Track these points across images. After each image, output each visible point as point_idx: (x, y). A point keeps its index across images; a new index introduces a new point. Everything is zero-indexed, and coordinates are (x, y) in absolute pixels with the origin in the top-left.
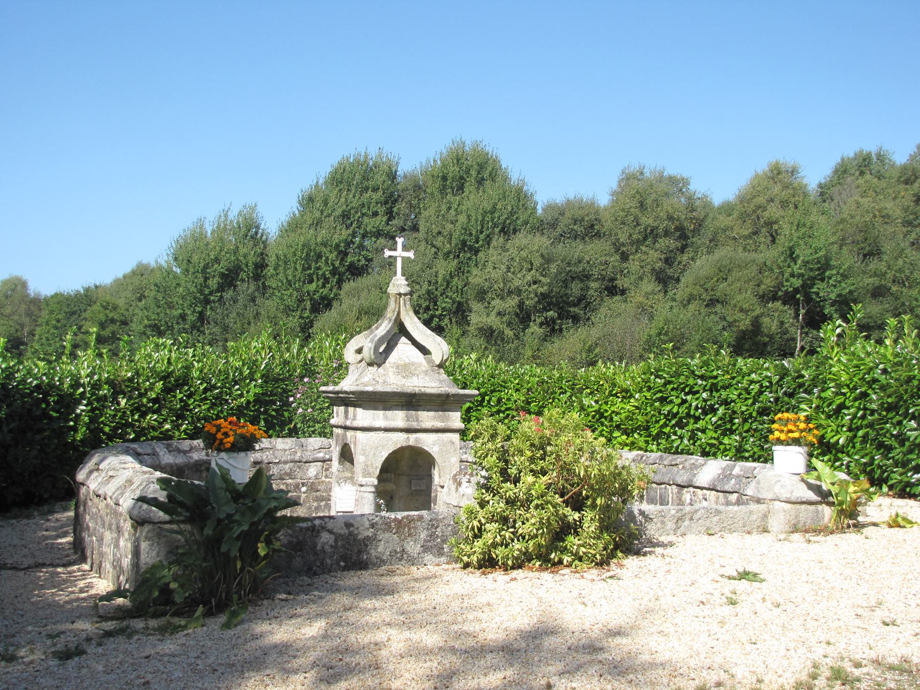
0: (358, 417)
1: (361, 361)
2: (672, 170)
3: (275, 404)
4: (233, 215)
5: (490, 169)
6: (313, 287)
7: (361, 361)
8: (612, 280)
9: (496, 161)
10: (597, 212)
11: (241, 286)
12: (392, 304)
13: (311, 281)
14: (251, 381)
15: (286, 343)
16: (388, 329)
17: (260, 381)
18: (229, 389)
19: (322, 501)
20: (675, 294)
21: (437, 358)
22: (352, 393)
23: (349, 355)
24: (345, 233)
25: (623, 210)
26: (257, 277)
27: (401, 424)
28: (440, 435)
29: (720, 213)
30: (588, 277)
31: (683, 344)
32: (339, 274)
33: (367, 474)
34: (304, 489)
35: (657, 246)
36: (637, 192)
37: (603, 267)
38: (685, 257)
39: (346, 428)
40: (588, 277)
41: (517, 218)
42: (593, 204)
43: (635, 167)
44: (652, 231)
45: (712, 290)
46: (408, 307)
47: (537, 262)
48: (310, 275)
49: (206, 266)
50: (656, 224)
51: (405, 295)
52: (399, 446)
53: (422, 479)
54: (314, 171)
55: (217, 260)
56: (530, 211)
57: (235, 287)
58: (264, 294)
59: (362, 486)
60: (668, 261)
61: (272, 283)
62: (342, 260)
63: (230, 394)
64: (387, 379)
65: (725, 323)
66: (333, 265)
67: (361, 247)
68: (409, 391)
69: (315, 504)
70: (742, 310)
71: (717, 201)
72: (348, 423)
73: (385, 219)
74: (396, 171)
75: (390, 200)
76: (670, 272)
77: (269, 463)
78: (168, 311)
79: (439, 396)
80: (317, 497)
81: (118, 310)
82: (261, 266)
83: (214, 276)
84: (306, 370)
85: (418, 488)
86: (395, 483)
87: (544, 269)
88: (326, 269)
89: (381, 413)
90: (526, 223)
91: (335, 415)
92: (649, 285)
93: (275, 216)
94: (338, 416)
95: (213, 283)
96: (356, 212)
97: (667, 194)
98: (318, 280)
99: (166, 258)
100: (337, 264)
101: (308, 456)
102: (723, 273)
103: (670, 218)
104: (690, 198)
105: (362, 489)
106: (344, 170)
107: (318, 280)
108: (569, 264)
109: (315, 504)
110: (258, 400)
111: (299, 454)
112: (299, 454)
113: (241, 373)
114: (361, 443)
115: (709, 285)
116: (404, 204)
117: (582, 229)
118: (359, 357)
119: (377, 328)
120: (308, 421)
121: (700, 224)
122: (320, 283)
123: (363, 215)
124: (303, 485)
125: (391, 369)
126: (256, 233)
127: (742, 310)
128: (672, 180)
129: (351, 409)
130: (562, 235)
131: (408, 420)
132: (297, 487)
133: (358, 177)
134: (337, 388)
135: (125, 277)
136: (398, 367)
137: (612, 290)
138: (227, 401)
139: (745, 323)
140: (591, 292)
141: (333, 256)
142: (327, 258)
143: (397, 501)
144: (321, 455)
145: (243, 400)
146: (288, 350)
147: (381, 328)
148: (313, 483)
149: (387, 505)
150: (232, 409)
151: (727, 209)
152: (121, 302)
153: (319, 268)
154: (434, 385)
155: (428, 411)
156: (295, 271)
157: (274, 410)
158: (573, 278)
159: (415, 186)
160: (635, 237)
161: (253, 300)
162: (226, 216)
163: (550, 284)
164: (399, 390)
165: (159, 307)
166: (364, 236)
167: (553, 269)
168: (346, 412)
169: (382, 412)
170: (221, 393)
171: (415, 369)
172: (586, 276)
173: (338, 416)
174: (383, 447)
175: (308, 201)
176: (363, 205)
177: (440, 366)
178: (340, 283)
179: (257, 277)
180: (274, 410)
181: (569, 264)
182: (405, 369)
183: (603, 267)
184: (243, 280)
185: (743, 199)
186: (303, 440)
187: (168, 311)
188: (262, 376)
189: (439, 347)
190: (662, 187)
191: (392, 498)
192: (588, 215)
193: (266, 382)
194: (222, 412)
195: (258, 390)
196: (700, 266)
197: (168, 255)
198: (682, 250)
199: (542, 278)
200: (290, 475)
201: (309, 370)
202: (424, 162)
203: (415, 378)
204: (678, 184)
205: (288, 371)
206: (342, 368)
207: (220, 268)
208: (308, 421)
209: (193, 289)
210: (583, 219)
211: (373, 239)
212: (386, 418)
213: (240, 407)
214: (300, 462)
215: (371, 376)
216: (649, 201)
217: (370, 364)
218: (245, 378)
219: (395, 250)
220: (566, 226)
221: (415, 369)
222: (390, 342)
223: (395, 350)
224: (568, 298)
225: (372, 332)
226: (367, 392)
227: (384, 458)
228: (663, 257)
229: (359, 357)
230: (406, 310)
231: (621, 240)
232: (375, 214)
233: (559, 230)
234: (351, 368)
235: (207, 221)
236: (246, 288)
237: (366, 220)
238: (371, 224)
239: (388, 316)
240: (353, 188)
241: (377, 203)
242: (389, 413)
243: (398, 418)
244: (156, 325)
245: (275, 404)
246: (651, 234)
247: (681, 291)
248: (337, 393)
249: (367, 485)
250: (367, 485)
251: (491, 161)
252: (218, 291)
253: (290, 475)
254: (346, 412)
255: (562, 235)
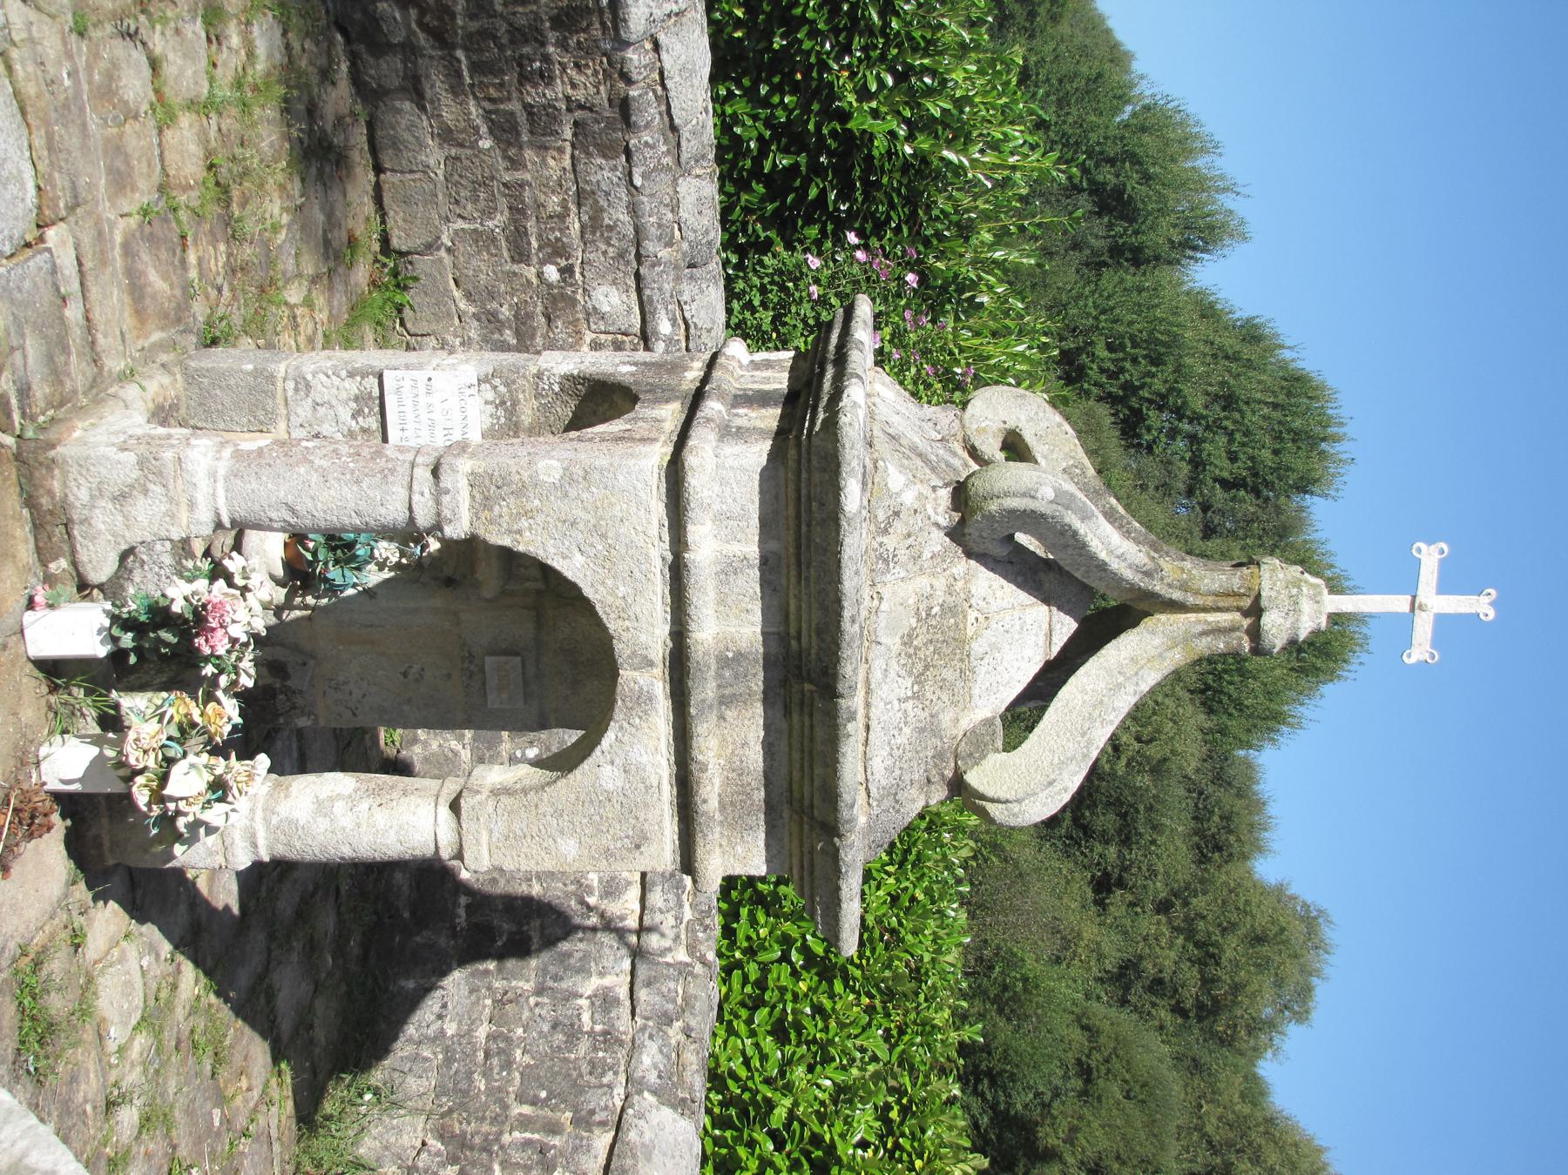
0: (731, 449)
1: (973, 452)
2: (1322, 992)
3: (841, 197)
4: (1227, 201)
5: (1319, 663)
6: (1102, 352)
7: (973, 452)
8: (1121, 884)
9: (1332, 675)
10: (1245, 857)
11: (1099, 226)
12: (1214, 578)
13: (1110, 348)
14: (907, 122)
15: (1022, 229)
16: (1114, 565)
17: (908, 150)
18: (883, 58)
19: (518, 334)
20: (1099, 998)
21: (992, 775)
22: (832, 423)
23: (997, 409)
24: (1197, 403)
25: (1247, 902)
26: (1116, 251)
27: (706, 633)
28: (668, 793)
29: (1245, 1077)
30: (1126, 842)
31: (1009, 1020)
32: (1125, 396)
33: (487, 490)
34: (552, 273)
35: (1185, 965)
36: (1283, 930)
37: (1144, 868)
38: (1164, 1015)
39: (697, 398)
40: (1126, 842)
41: (1230, 715)
42: (1260, 850)
43: (1328, 933)
44: (1212, 956)
45: (1109, 1071)
46: (1204, 646)
47: (1154, 751)
48: (1122, 347)
49: (1135, 160)
50: (1224, 962)
51: (1255, 633)
52: (612, 626)
53: (527, 696)
54: (1306, 346)
55: (1147, 178)
56: (1244, 738)
57: (1099, 215)
58: (1087, 265)
59: (435, 473)
60: (1157, 985)
61: (1109, 279)
62: (1150, 401)
63: (868, 61)
64: (898, 568)
65: (1047, 1098)
66: (1142, 387)
67: (1173, 433)
68: (847, 669)
69: (505, 312)
70: (1074, 1130)
71: (1266, 1068)
72: (713, 407)
73: (1225, 475)
74: (1312, 493)
75: (1254, 483)
76: (1138, 988)
77: (628, 153)
78: (1053, 98)
79: (830, 794)
80: (530, 316)
81: (1049, 24)
82: (1138, 258)
83: (1117, 176)
84: (944, 289)
85: (492, 682)
86: (504, 593)
87: (1140, 764)
88: (1132, 374)
89: (750, 548)
90: (1223, 731)
91: (762, 356)
92: (1114, 952)
93: (1223, 278)
94: (755, 366)
95: (1106, 175)
96: (1235, 422)
97: (1279, 984)
98: (1113, 361)
99: (1147, 93)
100: (1145, 393)
101: (661, 284)
102: (1141, 1092)
103: (1236, 988)
104: (1271, 1025)
105: (422, 474)
106: (1310, 398)
107: (1113, 361)
108: (1150, 809)
109: (505, 312)
110: (854, 144)
111: (664, 253)
112: (664, 253)
113: (929, 92)
114: (630, 461)
115: (1116, 1065)
116: (1252, 509)
117: (1214, 830)
118: (991, 447)
119: (1110, 515)
120: (783, 288)
121: (1226, 1042)
122: (1108, 365)
123: (1231, 435)
124: (567, 271)
125: (940, 583)
126: (1195, 248)
127: (1074, 1130)
128: (1305, 992)
129: (770, 417)
130: (1201, 793)
131: (724, 662)
132: (557, 251)
133: (1297, 423)
134: (861, 358)
135: (1108, 31)
136: (949, 610)
137: (1103, 886)
138: (847, 49)
139: (1049, 1137)
140: (1099, 848)
141: (1158, 385)
142: (1153, 376)
143: (438, 602)
144: (665, 327)
145: (851, 98)
146: (1002, 237)
147: (1115, 537)
148: (574, 302)
149: (419, 565)
150: (823, 66)
151: (1254, 1091)
152: (1064, 28)
153: (1135, 361)
154: (877, 765)
155: (769, 747)
156: (1130, 322)
157: (823, 193)
158: (1124, 816)
159: (1285, 528)
160: (1201, 925)
161: (1076, 246)
162: (1225, 190)
163: (1113, 774)
164: (849, 628)
165: (1060, 81)
166: (1192, 438)
167: (1143, 780)
168: (761, 399)
169: (752, 550)
170: (870, 31)
171: (943, 685)
172: (1128, 838)
173: (755, 366)
174: (606, 561)
175: (1252, 334)
176: (1247, 434)
177: (957, 786)
178: (1111, 399)
179: (1116, 251)
180: (823, 193)
181: (1150, 809)
182: (942, 644)
183: (1144, 868)
184: (1110, 226)
185: (1270, 1124)
186: (715, 266)
187: (1053, 98)
188: (923, 158)
189: (1033, 782)
190: (1291, 969)
191: (450, 582)
192: (1238, 840)
193: (906, 167)
194: (814, 33)
195: (880, 144)
196: (1152, 1048)
197: (1153, 95)
198: (1178, 1010)
199: (1123, 761)
200: (594, 226)
201: (939, 295)
202: (1328, 547)
203: (906, 686)
204: (1298, 1003)
205: (939, 235)
206: (945, 382)
207: (1133, 186)
208: (783, 288)
209: (1093, 137)
210: (1230, 832)
211: (1188, 455)
212: (729, 569)
213: (830, 93)
214: (638, 256)
215: (908, 498)
216: (1265, 949)
217: (961, 495)
218: (914, 104)
219: (1444, 588)
220: (1218, 801)
221: (943, 685)
222: (1051, 570)
223: (1023, 597)
224: (1088, 808)
225: (1094, 495)
226: (836, 490)
227: (557, 564)
228: (1166, 976)
229: (991, 447)
230: (1187, 639)
231: (1194, 901)
232: (1233, 457)
233: (1211, 789)
234: (945, 416)
235: (1215, 157)
236: (1097, 234)
237: (1222, 440)
238: (1215, 449)
239: (1167, 565)
240: (1277, 415)
241: (1252, 458)
242: (750, 583)
243: (731, 621)
244: (1029, 76)
245: (841, 197)
246: (1207, 955)
247: (1103, 1012)
248: (841, 360)
249: (439, 493)
250: (439, 493)
251: (1332, 665)
252: (1091, 181)
253: (594, 226)
254: (761, 399)
255: (1201, 793)
